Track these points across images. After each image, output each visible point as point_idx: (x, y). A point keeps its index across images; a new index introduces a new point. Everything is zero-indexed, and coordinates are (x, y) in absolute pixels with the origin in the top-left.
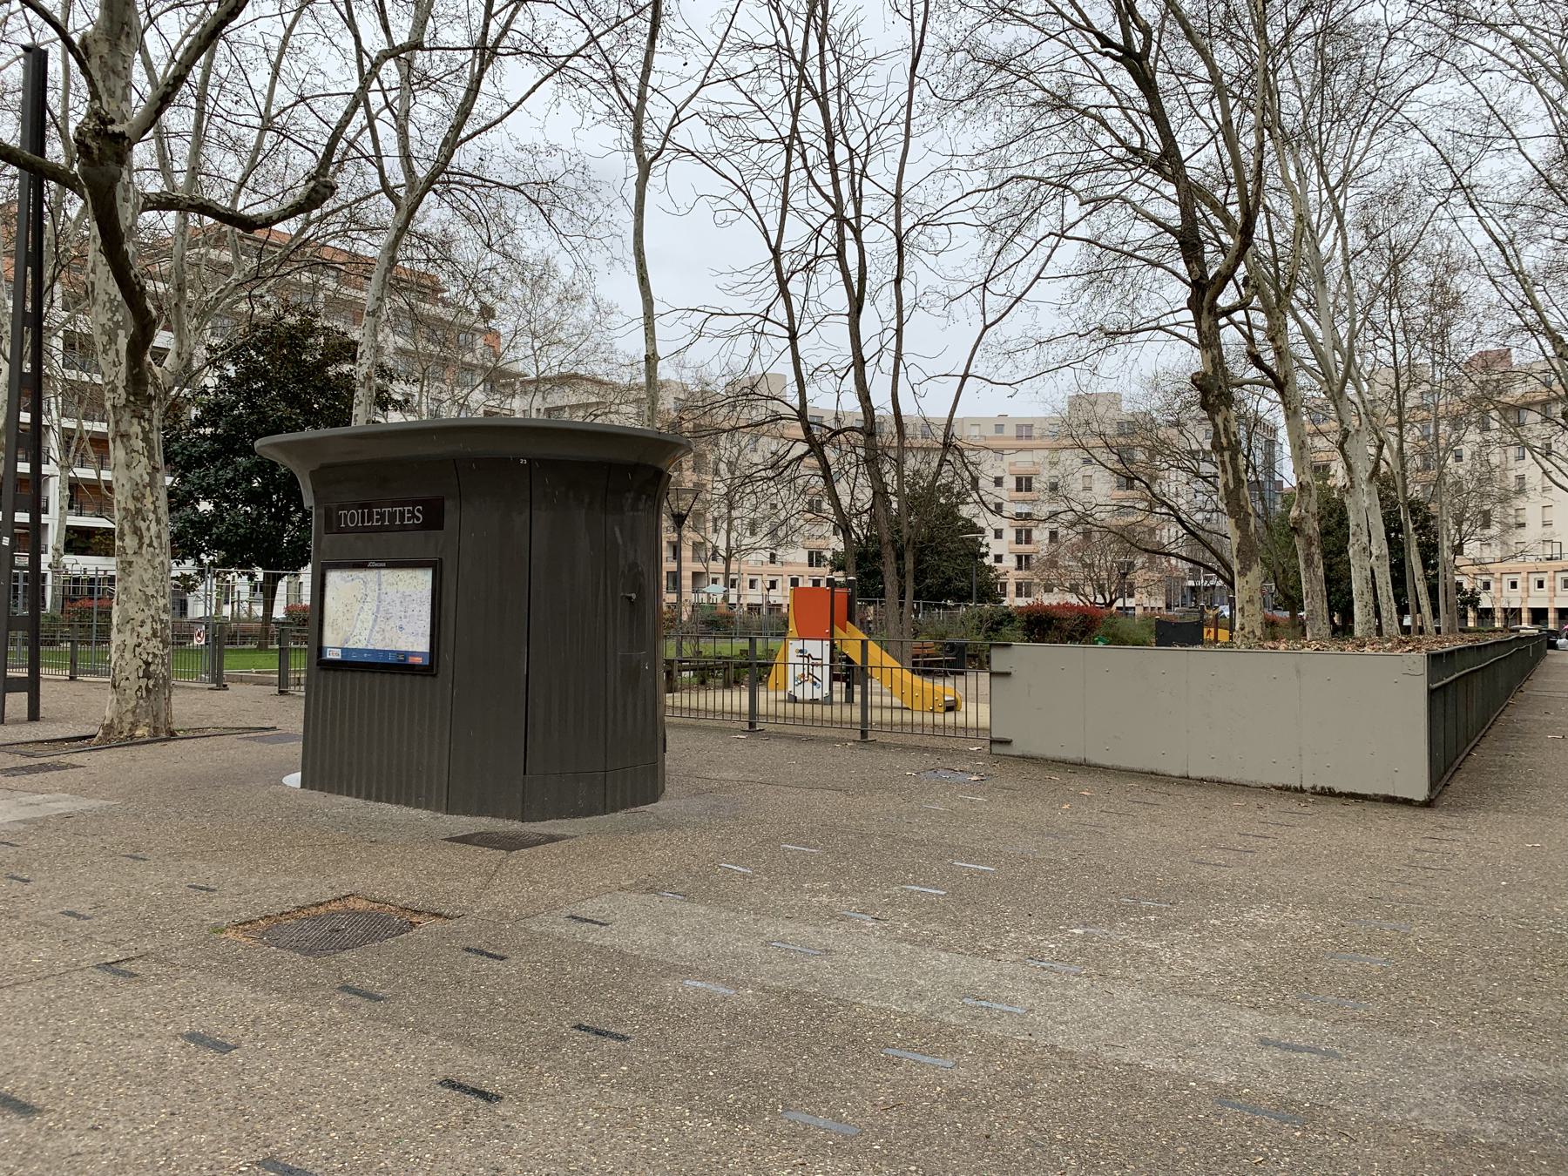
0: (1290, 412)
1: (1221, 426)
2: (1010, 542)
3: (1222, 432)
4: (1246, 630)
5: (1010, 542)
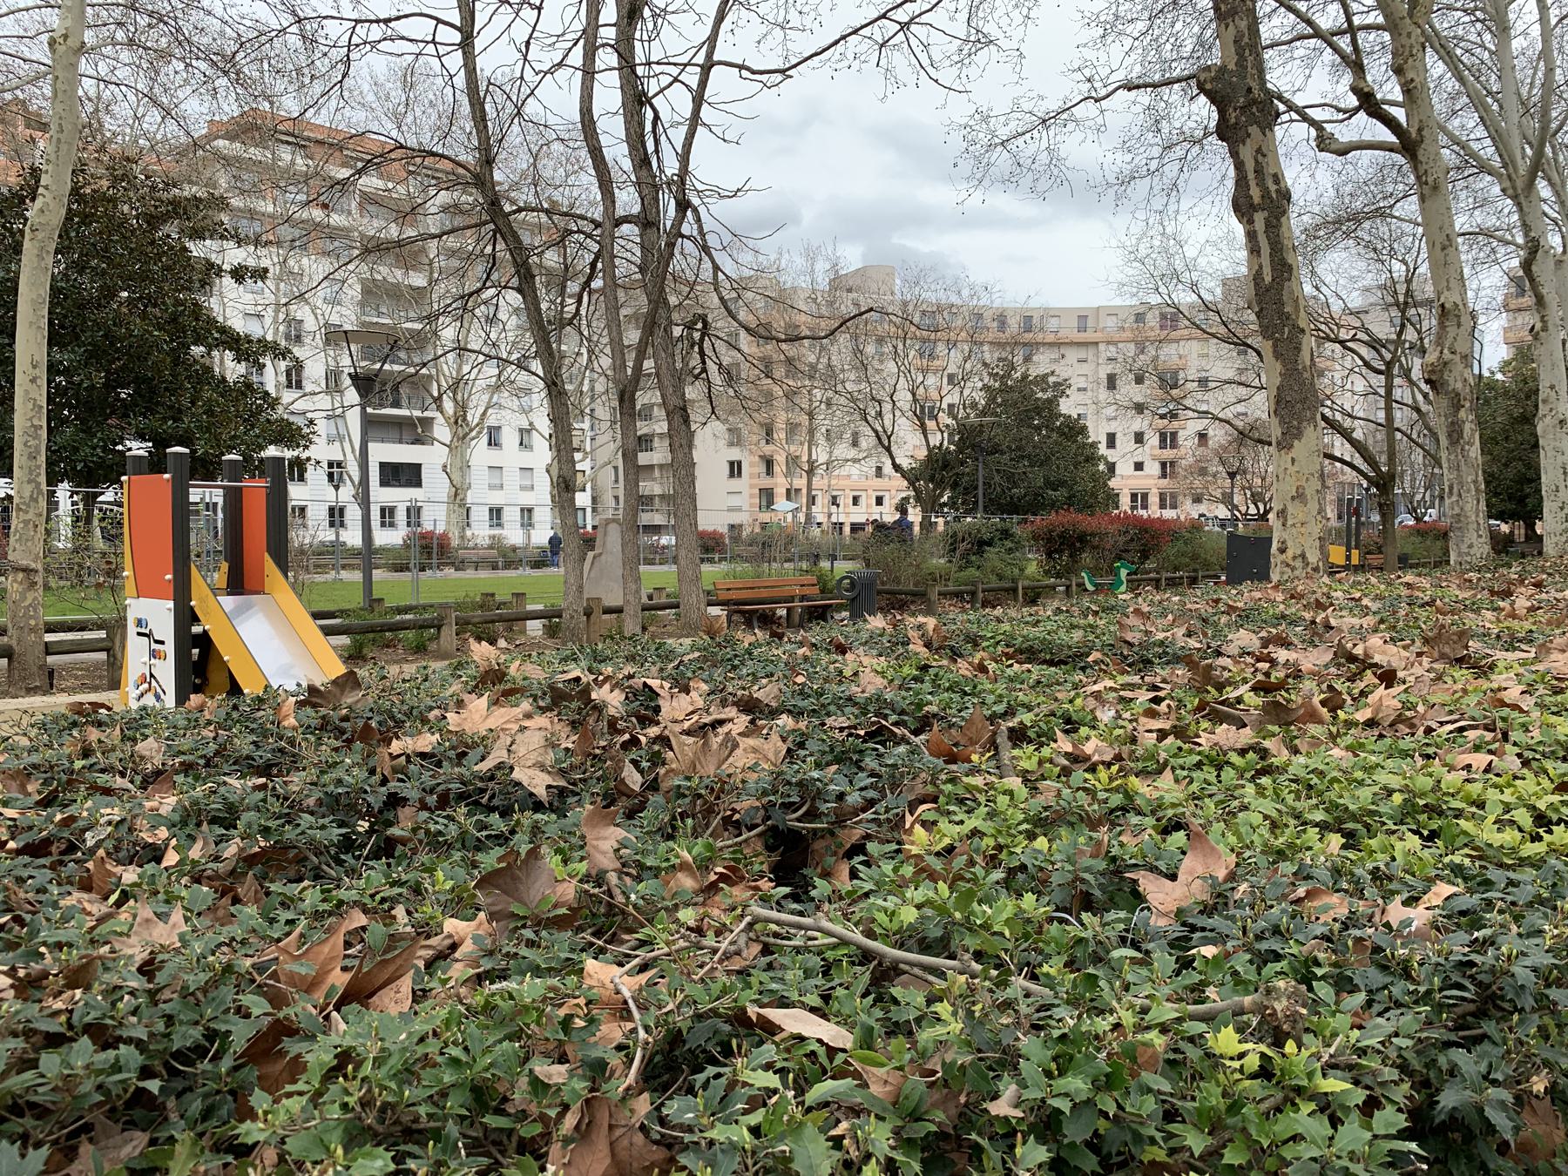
0: (1426, 190)
1: (1250, 166)
2: (1152, 447)
3: (1251, 176)
4: (1290, 553)
5: (1152, 447)
